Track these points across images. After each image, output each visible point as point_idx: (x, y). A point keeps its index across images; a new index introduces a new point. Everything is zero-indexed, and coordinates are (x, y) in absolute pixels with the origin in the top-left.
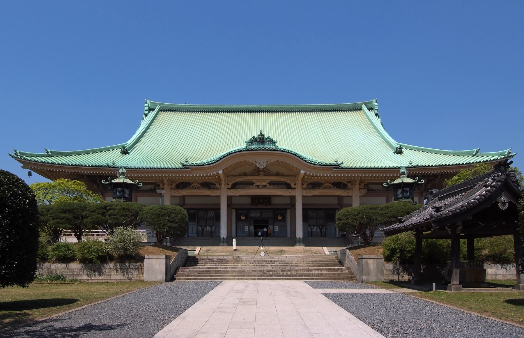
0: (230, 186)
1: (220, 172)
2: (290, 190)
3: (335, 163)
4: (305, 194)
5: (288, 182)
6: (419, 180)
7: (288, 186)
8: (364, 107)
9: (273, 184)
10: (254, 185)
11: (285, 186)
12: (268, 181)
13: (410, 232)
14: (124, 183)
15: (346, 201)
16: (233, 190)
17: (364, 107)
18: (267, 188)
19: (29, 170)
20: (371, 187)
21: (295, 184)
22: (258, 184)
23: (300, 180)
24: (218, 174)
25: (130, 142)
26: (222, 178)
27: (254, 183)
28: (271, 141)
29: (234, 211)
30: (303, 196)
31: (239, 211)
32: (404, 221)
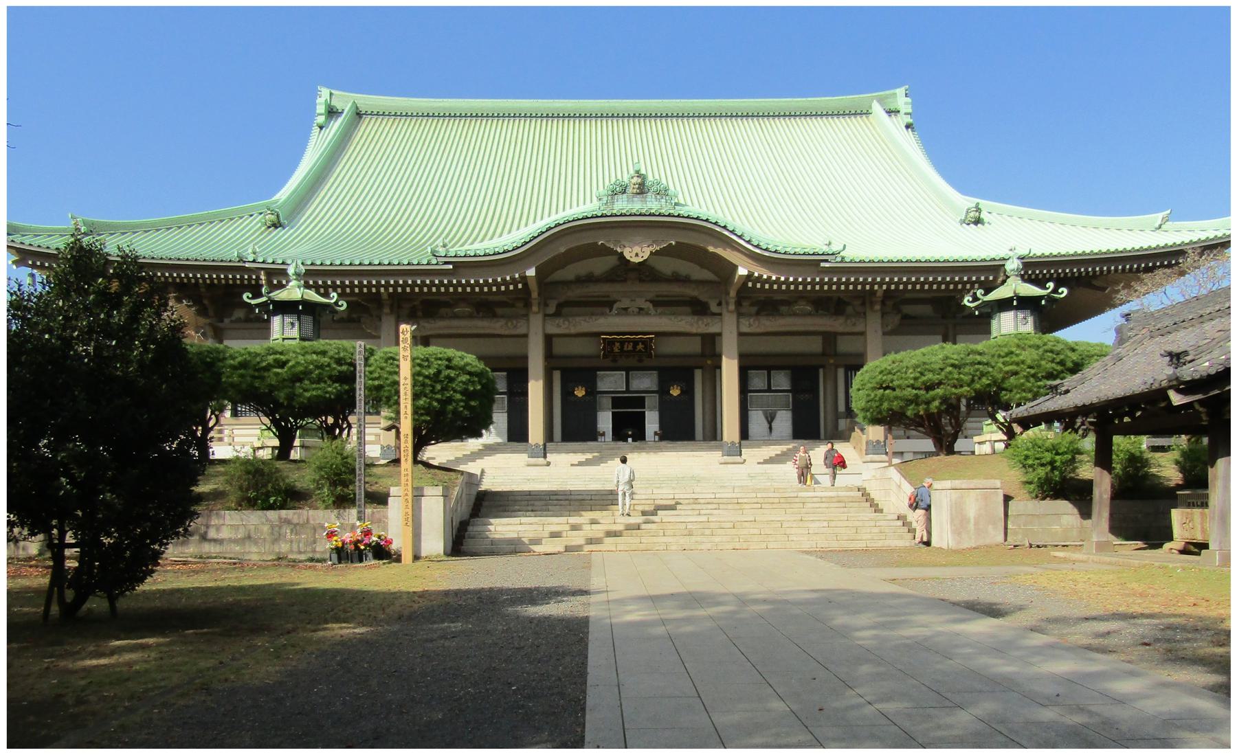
0: (551, 309)
1: (531, 272)
2: (707, 320)
3: (825, 249)
4: (745, 329)
5: (703, 298)
6: (1055, 291)
7: (699, 308)
8: (877, 108)
9: (661, 303)
10: (616, 306)
11: (688, 309)
12: (651, 296)
13: (217, 456)
14: (304, 302)
15: (844, 346)
16: (560, 321)
17: (877, 108)
18: (648, 314)
19: (29, 270)
20: (909, 309)
21: (720, 304)
22: (625, 303)
23: (733, 293)
24: (524, 279)
25: (283, 195)
26: (533, 286)
27: (615, 302)
28: (663, 193)
29: (557, 376)
30: (741, 334)
31: (571, 374)
32: (1067, 392)
